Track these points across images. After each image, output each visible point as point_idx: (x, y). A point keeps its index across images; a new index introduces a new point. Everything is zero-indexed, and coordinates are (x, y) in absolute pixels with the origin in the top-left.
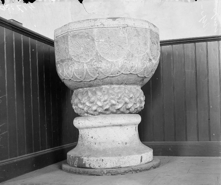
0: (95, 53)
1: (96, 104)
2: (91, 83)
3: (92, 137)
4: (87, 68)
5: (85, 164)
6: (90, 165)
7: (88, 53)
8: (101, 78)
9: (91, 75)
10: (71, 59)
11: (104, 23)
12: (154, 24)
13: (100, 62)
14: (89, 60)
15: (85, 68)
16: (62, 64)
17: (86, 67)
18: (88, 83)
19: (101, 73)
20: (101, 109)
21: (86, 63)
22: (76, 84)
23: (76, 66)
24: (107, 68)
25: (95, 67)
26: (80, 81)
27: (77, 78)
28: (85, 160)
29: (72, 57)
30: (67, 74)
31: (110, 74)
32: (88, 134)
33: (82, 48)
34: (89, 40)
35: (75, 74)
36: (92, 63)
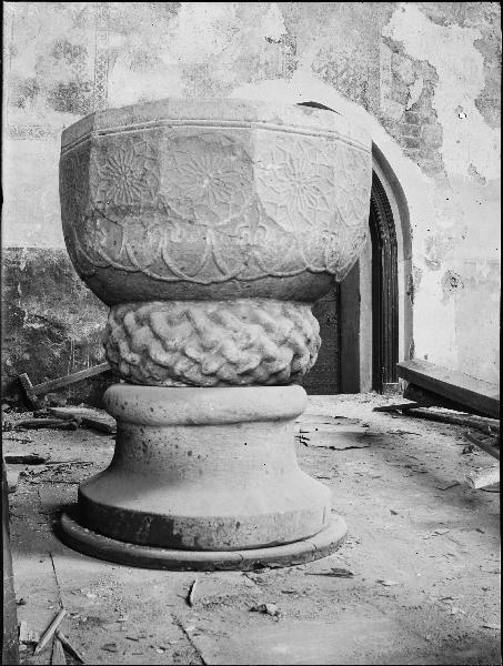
0: (248, 202)
1: (220, 353)
2: (213, 288)
3: (190, 454)
4: (214, 242)
5: (179, 537)
6: (196, 539)
7: (226, 197)
8: (249, 278)
9: (223, 265)
10: (165, 211)
11: (283, 118)
12: (323, 110)
13: (260, 231)
14: (226, 221)
15: (208, 243)
16: (117, 219)
17: (211, 238)
18: (200, 287)
19: (256, 262)
20: (231, 369)
21: (216, 229)
22: (150, 285)
23: (178, 233)
24: (276, 251)
25: (242, 242)
26: (174, 278)
27: (169, 269)
28: (180, 526)
29: (169, 204)
30: (131, 253)
31: (277, 266)
32: (175, 442)
33: (206, 181)
34: (233, 158)
35: (166, 257)
36: (233, 231)
